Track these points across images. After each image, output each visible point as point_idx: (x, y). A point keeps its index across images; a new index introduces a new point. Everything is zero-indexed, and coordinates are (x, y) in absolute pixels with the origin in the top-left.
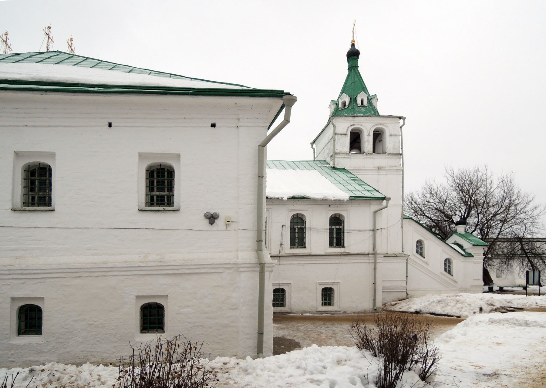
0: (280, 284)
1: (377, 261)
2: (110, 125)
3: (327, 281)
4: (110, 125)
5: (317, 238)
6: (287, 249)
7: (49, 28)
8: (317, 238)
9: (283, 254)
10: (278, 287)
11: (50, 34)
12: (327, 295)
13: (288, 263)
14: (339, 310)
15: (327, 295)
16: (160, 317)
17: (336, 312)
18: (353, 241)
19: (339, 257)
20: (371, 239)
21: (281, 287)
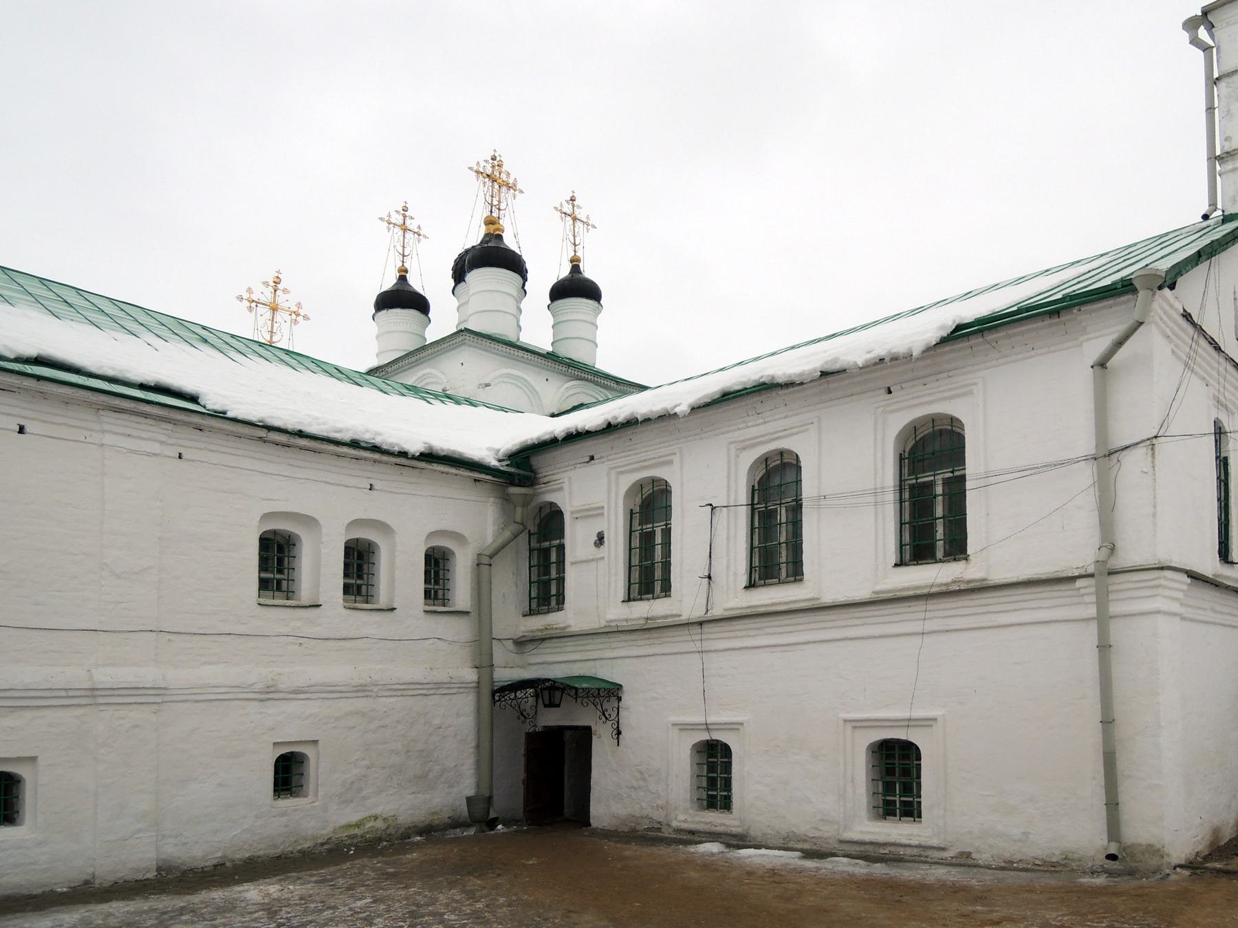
0: (707, 727)
1: (1114, 608)
2: (21, 430)
3: (891, 713)
4: (21, 430)
5: (851, 537)
6: (733, 593)
7: (573, 199)
8: (851, 537)
9: (717, 612)
10: (705, 736)
11: (577, 211)
12: (897, 770)
13: (657, 650)
14: (935, 842)
15: (897, 770)
16: (888, 779)
17: (922, 855)
18: (1006, 526)
19: (920, 606)
20: (1089, 501)
21: (716, 736)
